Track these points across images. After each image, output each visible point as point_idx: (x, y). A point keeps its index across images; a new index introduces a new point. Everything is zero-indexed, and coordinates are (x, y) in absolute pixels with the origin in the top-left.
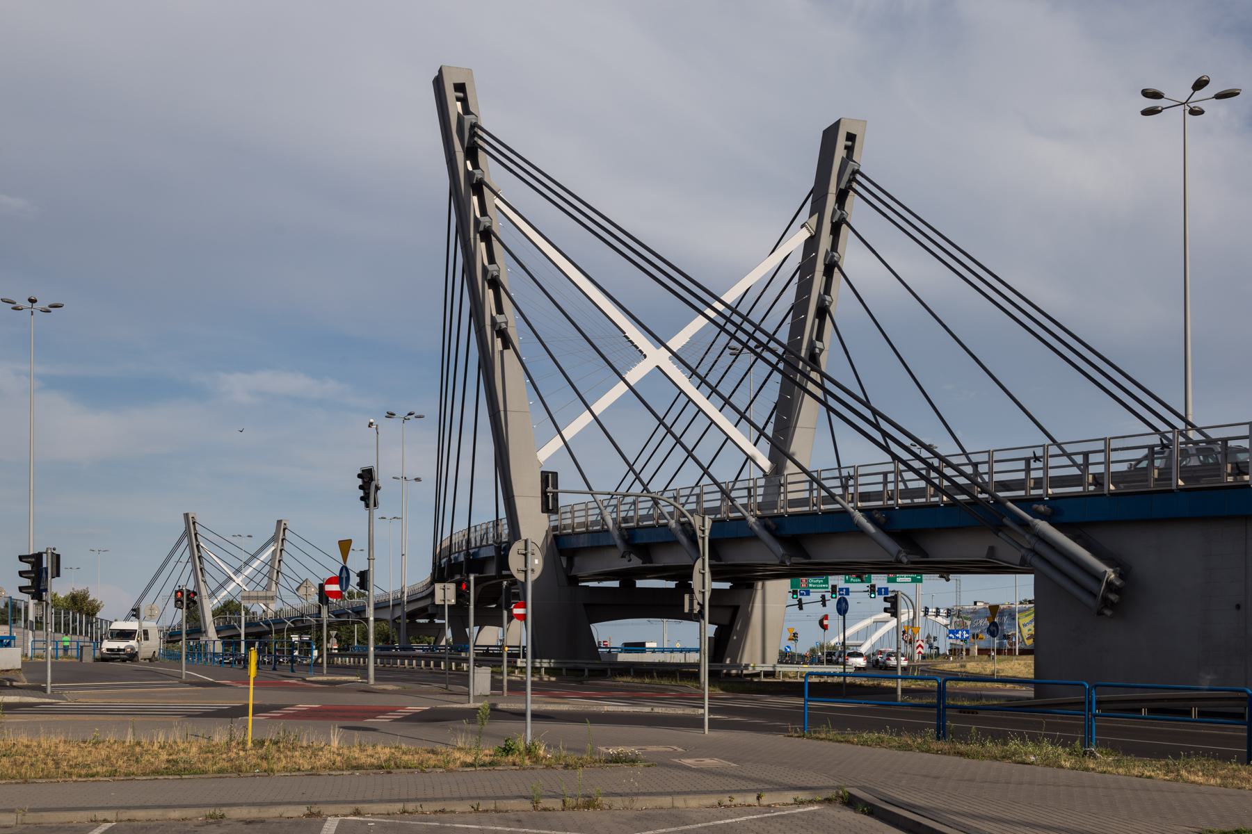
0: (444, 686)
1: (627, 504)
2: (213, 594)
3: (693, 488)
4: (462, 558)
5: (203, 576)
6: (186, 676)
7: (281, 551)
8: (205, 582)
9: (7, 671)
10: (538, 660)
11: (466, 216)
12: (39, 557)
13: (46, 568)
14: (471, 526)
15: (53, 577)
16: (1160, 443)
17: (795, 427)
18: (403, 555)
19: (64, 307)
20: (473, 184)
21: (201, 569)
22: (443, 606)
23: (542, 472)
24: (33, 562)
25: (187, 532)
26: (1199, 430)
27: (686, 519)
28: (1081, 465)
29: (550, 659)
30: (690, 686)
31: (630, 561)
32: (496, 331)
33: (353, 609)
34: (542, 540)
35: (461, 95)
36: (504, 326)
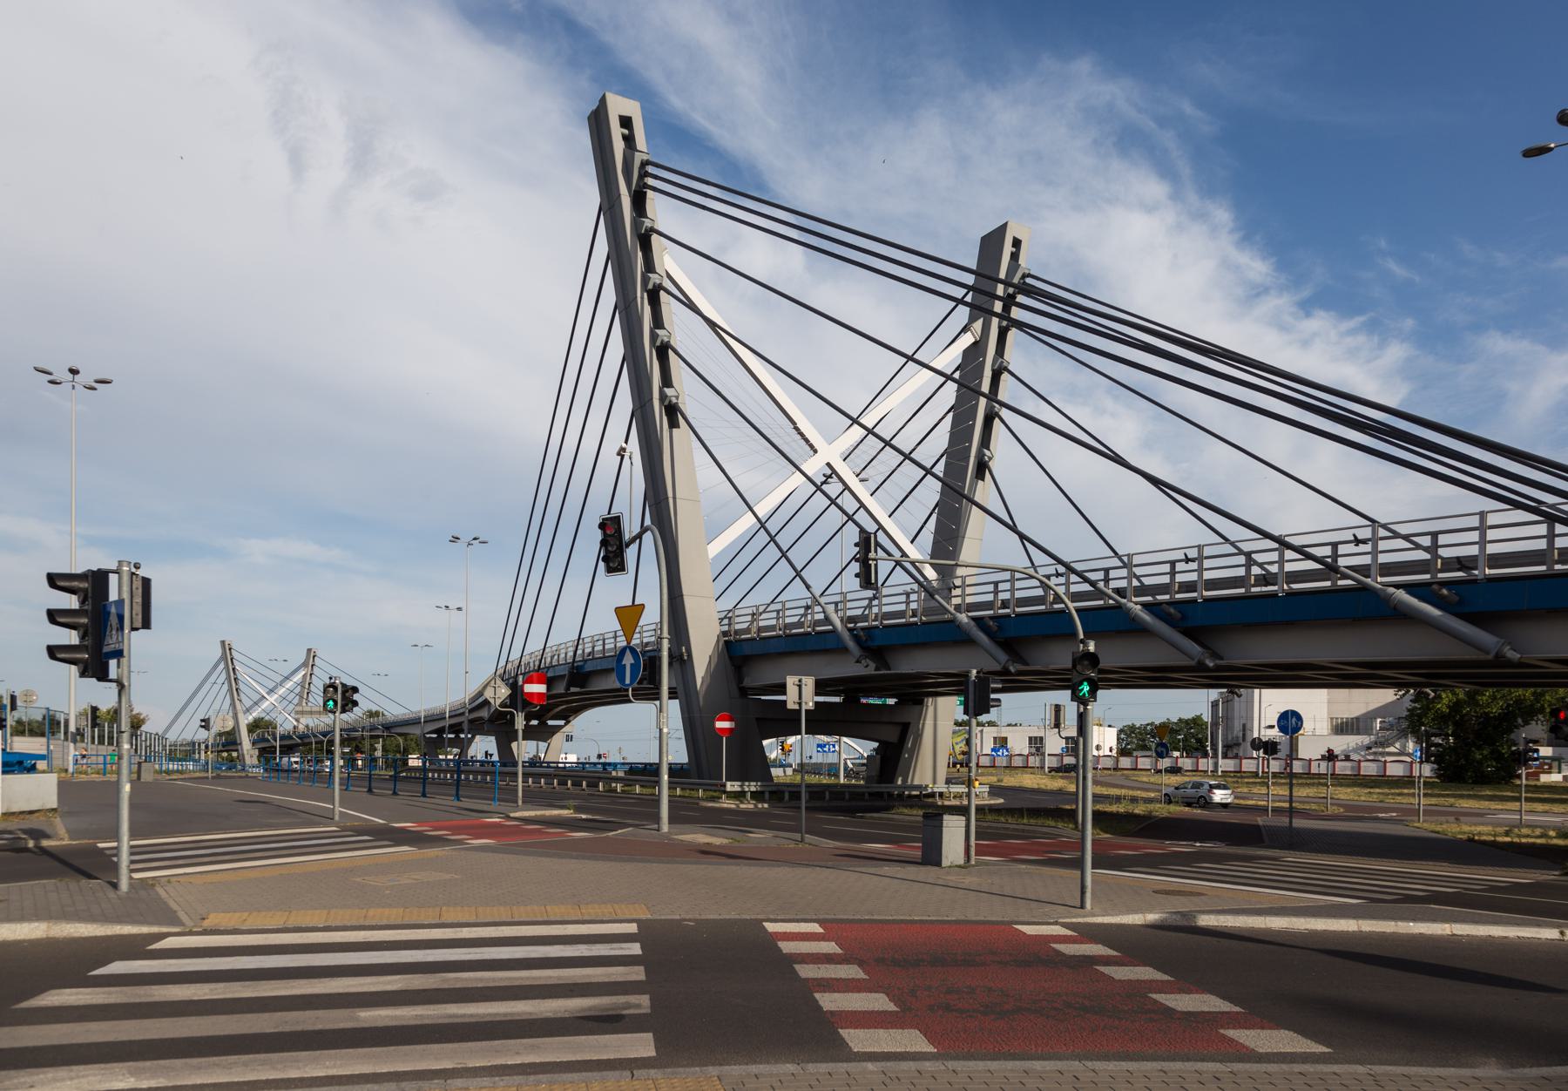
0: (798, 836)
2: (248, 710)
5: (238, 695)
6: (340, 817)
7: (311, 675)
8: (240, 701)
9: (31, 812)
10: (747, 783)
11: (631, 266)
12: (98, 579)
13: (120, 602)
15: (134, 629)
17: (964, 537)
18: (467, 673)
19: (113, 383)
20: (641, 234)
21: (237, 690)
22: (799, 711)
24: (85, 591)
25: (224, 657)
27: (1062, 606)
29: (757, 781)
30: (1064, 829)
32: (665, 406)
33: (382, 725)
34: (713, 645)
35: (626, 132)
36: (674, 400)
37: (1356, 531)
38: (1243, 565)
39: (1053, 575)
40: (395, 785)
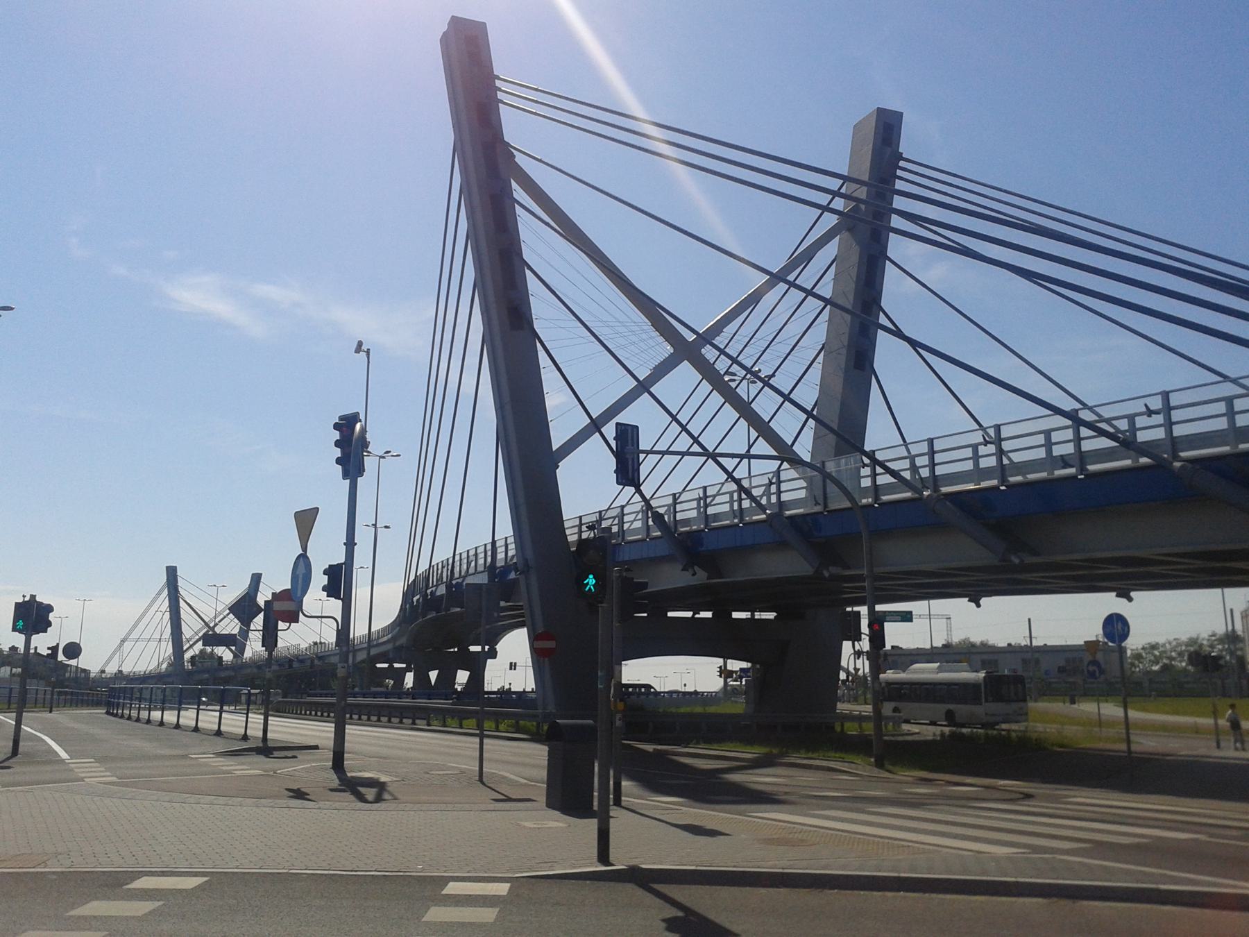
1: (610, 518)
3: (723, 484)
4: (442, 590)
14: (456, 553)
16: (983, 440)
23: (167, 567)
26: (1091, 409)
28: (1126, 431)
31: (694, 574)
37: (1147, 401)
38: (970, 459)
39: (980, 444)
40: (265, 731)
